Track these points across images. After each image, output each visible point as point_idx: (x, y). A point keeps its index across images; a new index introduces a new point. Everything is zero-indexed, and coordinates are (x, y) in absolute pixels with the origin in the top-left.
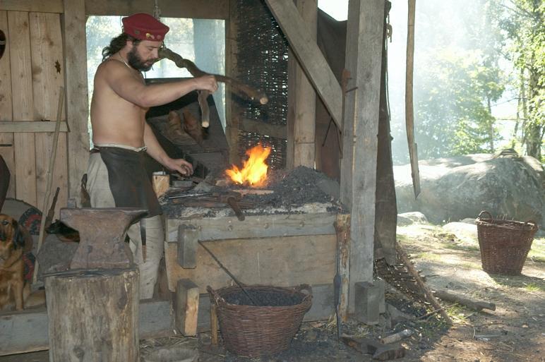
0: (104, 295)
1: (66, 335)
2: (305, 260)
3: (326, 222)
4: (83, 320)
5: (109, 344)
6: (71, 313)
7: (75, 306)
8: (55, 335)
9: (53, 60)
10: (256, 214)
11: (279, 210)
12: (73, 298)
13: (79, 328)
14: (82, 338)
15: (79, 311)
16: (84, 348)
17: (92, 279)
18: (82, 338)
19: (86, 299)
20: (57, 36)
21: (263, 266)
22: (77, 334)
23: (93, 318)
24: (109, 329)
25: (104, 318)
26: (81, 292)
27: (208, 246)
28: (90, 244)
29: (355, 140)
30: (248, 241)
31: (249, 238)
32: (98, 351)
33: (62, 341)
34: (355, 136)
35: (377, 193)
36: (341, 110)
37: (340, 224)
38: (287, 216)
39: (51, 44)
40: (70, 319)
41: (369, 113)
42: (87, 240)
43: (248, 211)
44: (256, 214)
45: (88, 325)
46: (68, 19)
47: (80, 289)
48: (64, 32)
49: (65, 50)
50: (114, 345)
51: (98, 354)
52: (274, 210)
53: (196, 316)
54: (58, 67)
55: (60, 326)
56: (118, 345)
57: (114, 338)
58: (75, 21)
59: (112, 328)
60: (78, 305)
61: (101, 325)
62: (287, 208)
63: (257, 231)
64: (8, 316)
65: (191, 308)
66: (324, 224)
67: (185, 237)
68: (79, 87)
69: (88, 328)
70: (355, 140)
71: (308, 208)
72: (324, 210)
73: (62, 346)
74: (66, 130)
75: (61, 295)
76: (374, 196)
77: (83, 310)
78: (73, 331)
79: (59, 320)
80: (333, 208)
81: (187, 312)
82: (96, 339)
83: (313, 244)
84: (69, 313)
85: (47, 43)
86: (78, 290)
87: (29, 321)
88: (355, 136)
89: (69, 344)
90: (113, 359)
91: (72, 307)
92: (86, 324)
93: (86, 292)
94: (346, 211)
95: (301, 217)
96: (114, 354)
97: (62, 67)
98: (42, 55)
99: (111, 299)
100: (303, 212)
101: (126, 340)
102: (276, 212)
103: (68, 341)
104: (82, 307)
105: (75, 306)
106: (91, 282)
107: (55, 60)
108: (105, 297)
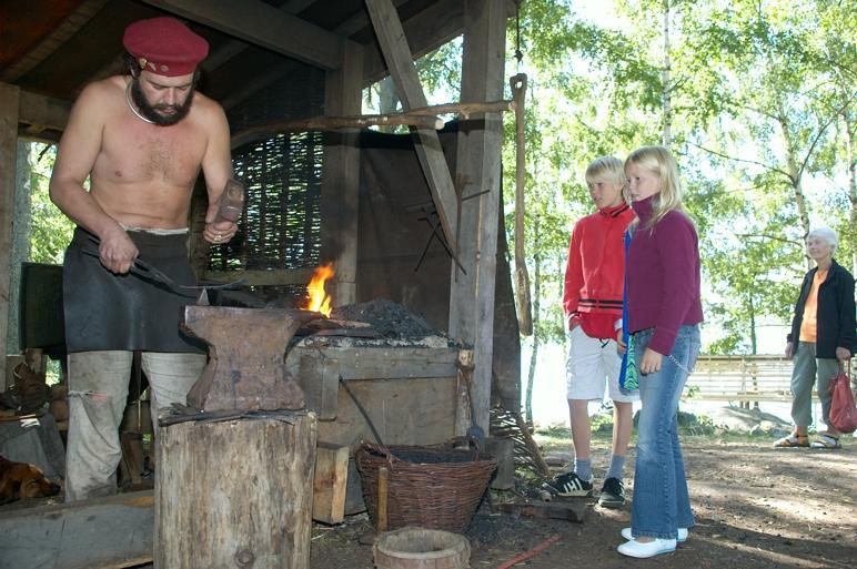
0: (288, 451)
3: (449, 361)
4: (255, 497)
5: (291, 540)
8: (191, 532)
10: (380, 346)
12: (236, 459)
15: (247, 482)
17: (272, 422)
18: (252, 531)
19: (260, 458)
22: (241, 526)
25: (286, 494)
26: (252, 446)
27: (349, 385)
28: (235, 368)
29: (479, 256)
41: (491, 227)
42: (753, 96)
45: (263, 508)
47: (252, 440)
52: (395, 343)
55: (205, 514)
59: (297, 510)
61: (281, 506)
62: (408, 340)
63: (385, 370)
64: (57, 512)
69: (263, 512)
70: (479, 256)
71: (429, 341)
72: (445, 346)
75: (212, 454)
77: (256, 479)
78: (235, 520)
79: (204, 503)
81: (335, 486)
82: (274, 532)
83: (434, 390)
87: (91, 519)
89: (226, 544)
90: (294, 566)
92: (260, 504)
93: (262, 447)
95: (426, 352)
99: (297, 457)
100: (427, 347)
102: (399, 346)
103: (222, 541)
106: (271, 426)
108: (288, 455)
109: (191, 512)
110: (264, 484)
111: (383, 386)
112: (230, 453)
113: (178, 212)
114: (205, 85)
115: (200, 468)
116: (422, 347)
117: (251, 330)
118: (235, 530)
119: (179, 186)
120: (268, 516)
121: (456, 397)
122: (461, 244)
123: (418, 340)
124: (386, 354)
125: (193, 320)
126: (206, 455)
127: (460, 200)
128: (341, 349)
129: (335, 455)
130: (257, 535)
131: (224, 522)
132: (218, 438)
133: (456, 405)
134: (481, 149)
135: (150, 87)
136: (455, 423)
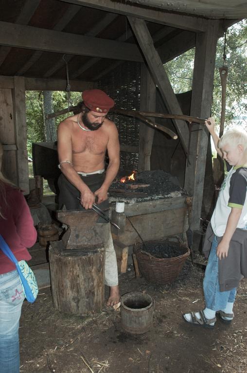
1: (67, 290)
2: (171, 222)
5: (93, 293)
6: (71, 278)
7: (73, 274)
9: (8, 113)
10: (149, 200)
11: (159, 197)
12: (71, 269)
13: (75, 286)
14: (78, 292)
16: (79, 298)
18: (78, 292)
20: (10, 100)
21: (152, 228)
22: (74, 290)
23: (85, 280)
24: (93, 285)
25: (90, 280)
26: (77, 266)
29: (197, 157)
30: (145, 215)
31: (146, 214)
32: (87, 298)
33: (65, 294)
34: (197, 156)
35: (204, 185)
36: (188, 141)
37: (188, 202)
38: (164, 200)
39: (7, 104)
40: (70, 281)
43: (145, 199)
44: (149, 200)
46: (17, 91)
48: (15, 99)
49: (15, 107)
50: (96, 293)
51: (87, 300)
53: (126, 263)
54: (11, 116)
55: (63, 285)
56: (97, 292)
57: (96, 289)
58: (20, 93)
60: (75, 274)
61: (89, 284)
62: (163, 195)
65: (124, 258)
66: (180, 203)
67: (119, 218)
68: (22, 126)
69: (81, 286)
70: (197, 157)
71: (173, 194)
72: (180, 195)
73: (65, 296)
74: (16, 149)
75: (63, 267)
76: (203, 186)
77: (78, 276)
78: (72, 288)
80: (184, 193)
84: (69, 277)
85: (5, 105)
86: (75, 264)
88: (197, 156)
91: (71, 274)
92: (80, 284)
93: (80, 265)
94: (191, 195)
95: (170, 200)
96: (96, 298)
97: (13, 116)
98: (3, 110)
99: (94, 267)
100: (171, 197)
101: (101, 288)
103: (68, 294)
104: (77, 274)
105: (73, 274)
107: (10, 112)
109: (58, 283)
110: (82, 277)
111: (149, 216)
112: (69, 268)
113: (97, 164)
114: (111, 115)
115: (60, 271)
116: (168, 198)
117: (82, 218)
118: (72, 291)
119: (96, 154)
120: (83, 287)
121: (185, 215)
122: (190, 150)
123: (167, 194)
124: (151, 203)
125: (61, 217)
126: (61, 267)
127: (190, 131)
128: (130, 205)
129: (122, 250)
130: (80, 293)
131: (69, 288)
132: (65, 263)
133: (184, 218)
134: (200, 109)
135: (93, 117)
136: (183, 225)
